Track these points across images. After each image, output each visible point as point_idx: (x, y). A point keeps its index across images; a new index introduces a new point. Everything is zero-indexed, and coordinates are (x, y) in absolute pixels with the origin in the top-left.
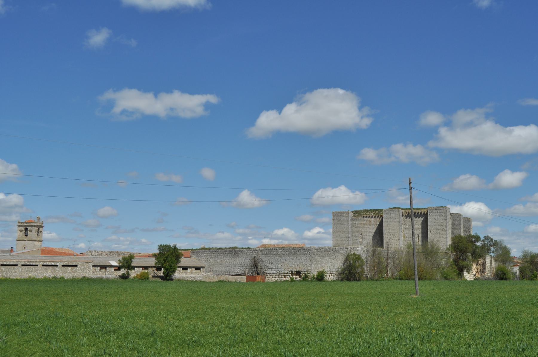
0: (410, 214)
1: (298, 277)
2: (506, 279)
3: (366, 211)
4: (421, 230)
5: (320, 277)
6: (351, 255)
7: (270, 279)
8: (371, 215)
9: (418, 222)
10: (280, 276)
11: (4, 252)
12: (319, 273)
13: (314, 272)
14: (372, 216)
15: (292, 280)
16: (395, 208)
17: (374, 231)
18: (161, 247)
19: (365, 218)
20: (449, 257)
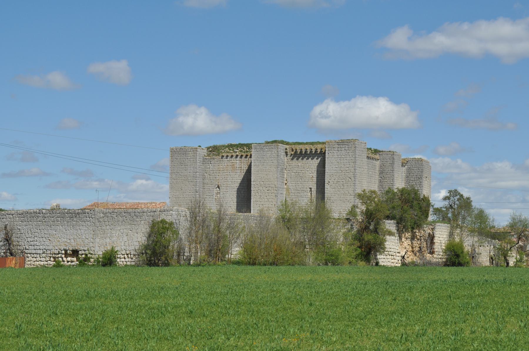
1: (75, 259)
2: (460, 264)
4: (315, 179)
5: (109, 260)
6: (158, 222)
7: (31, 262)
8: (234, 154)
13: (99, 251)
15: (58, 265)
16: (275, 142)
17: (239, 181)
18: (468, 198)
20: (352, 228)
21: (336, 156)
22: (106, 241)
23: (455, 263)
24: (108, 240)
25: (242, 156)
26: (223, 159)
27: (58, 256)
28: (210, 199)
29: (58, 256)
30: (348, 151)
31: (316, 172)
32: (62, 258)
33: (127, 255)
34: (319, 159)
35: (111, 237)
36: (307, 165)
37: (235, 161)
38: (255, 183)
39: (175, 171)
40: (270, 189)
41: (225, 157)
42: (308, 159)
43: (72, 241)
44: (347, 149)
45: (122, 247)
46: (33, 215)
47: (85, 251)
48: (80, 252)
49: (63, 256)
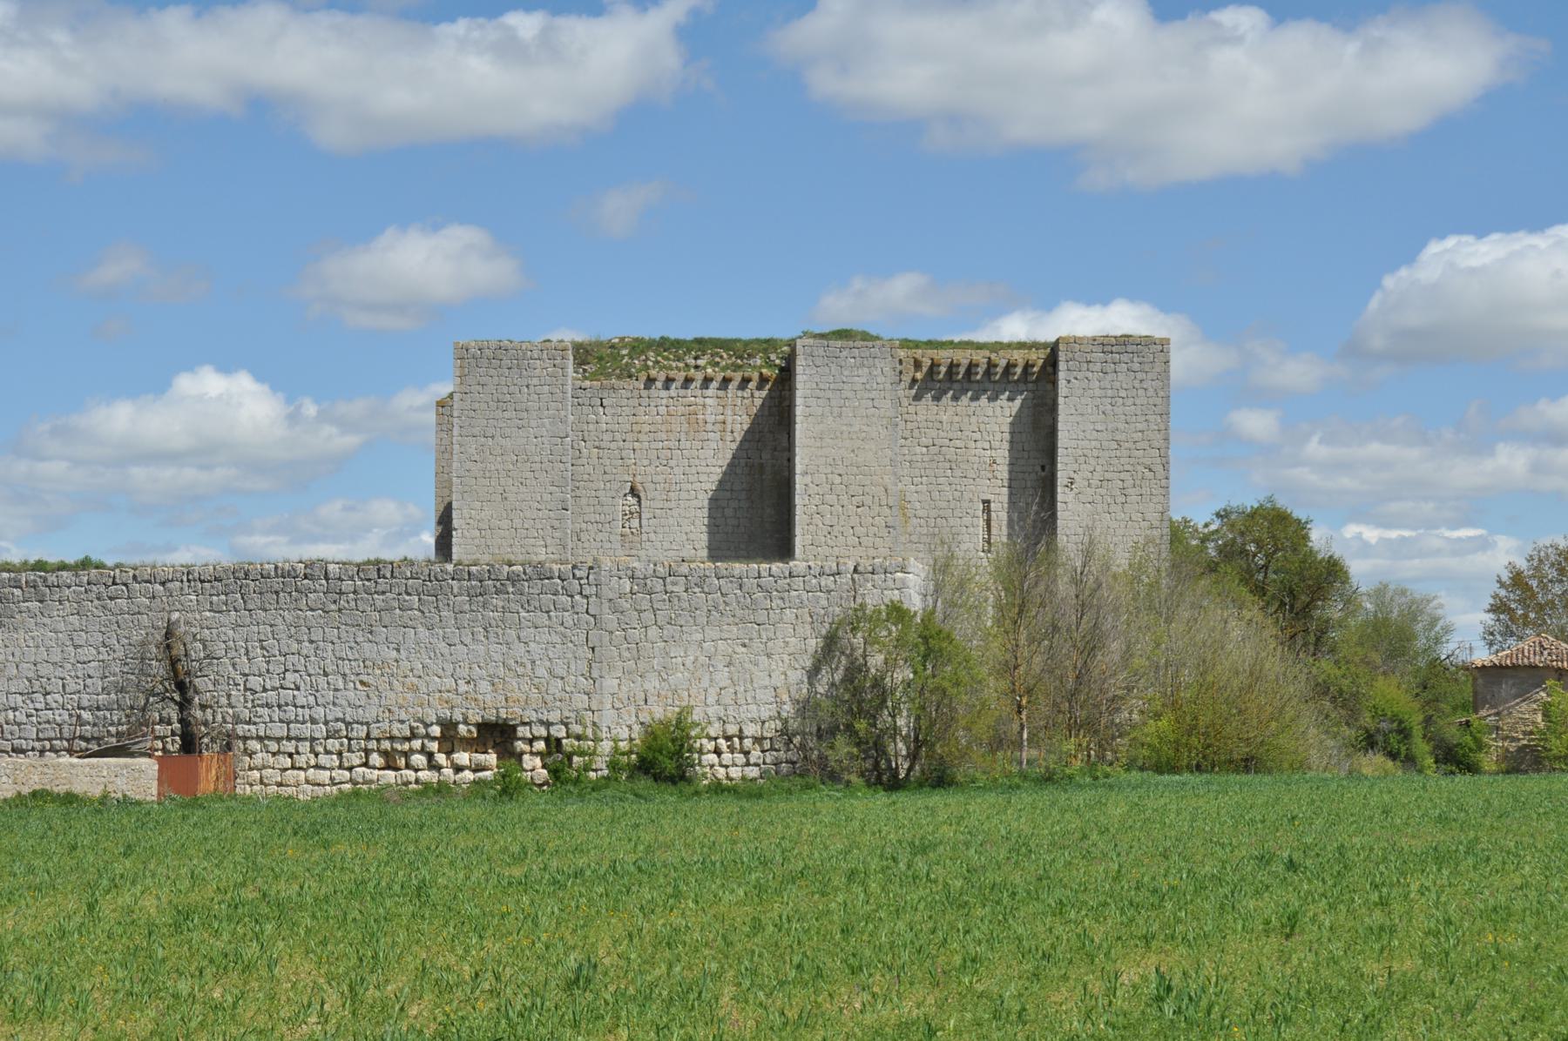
0: (946, 377)
3: (664, 345)
4: (1003, 472)
5: (662, 762)
7: (263, 774)
9: (996, 417)
10: (356, 759)
11: (7, 567)
12: (651, 733)
13: (618, 728)
14: (707, 381)
17: (717, 473)
19: (658, 391)
21: (1098, 392)
22: (647, 686)
23: (1398, 753)
24: (652, 684)
25: (726, 381)
26: (653, 392)
27: (406, 746)
28: (600, 536)
29: (406, 746)
30: (1140, 376)
31: (1006, 446)
32: (430, 756)
33: (728, 738)
34: (1018, 402)
35: (664, 672)
36: (974, 419)
37: (700, 400)
38: (808, 479)
39: (476, 431)
40: (868, 500)
41: (659, 384)
42: (975, 398)
43: (484, 686)
44: (1136, 366)
45: (710, 711)
46: (277, 583)
47: (548, 724)
48: (523, 731)
49: (434, 746)
